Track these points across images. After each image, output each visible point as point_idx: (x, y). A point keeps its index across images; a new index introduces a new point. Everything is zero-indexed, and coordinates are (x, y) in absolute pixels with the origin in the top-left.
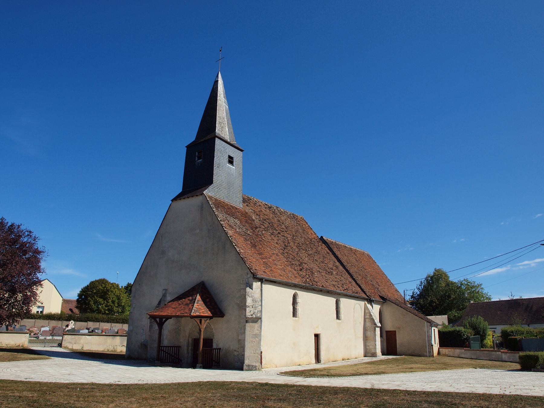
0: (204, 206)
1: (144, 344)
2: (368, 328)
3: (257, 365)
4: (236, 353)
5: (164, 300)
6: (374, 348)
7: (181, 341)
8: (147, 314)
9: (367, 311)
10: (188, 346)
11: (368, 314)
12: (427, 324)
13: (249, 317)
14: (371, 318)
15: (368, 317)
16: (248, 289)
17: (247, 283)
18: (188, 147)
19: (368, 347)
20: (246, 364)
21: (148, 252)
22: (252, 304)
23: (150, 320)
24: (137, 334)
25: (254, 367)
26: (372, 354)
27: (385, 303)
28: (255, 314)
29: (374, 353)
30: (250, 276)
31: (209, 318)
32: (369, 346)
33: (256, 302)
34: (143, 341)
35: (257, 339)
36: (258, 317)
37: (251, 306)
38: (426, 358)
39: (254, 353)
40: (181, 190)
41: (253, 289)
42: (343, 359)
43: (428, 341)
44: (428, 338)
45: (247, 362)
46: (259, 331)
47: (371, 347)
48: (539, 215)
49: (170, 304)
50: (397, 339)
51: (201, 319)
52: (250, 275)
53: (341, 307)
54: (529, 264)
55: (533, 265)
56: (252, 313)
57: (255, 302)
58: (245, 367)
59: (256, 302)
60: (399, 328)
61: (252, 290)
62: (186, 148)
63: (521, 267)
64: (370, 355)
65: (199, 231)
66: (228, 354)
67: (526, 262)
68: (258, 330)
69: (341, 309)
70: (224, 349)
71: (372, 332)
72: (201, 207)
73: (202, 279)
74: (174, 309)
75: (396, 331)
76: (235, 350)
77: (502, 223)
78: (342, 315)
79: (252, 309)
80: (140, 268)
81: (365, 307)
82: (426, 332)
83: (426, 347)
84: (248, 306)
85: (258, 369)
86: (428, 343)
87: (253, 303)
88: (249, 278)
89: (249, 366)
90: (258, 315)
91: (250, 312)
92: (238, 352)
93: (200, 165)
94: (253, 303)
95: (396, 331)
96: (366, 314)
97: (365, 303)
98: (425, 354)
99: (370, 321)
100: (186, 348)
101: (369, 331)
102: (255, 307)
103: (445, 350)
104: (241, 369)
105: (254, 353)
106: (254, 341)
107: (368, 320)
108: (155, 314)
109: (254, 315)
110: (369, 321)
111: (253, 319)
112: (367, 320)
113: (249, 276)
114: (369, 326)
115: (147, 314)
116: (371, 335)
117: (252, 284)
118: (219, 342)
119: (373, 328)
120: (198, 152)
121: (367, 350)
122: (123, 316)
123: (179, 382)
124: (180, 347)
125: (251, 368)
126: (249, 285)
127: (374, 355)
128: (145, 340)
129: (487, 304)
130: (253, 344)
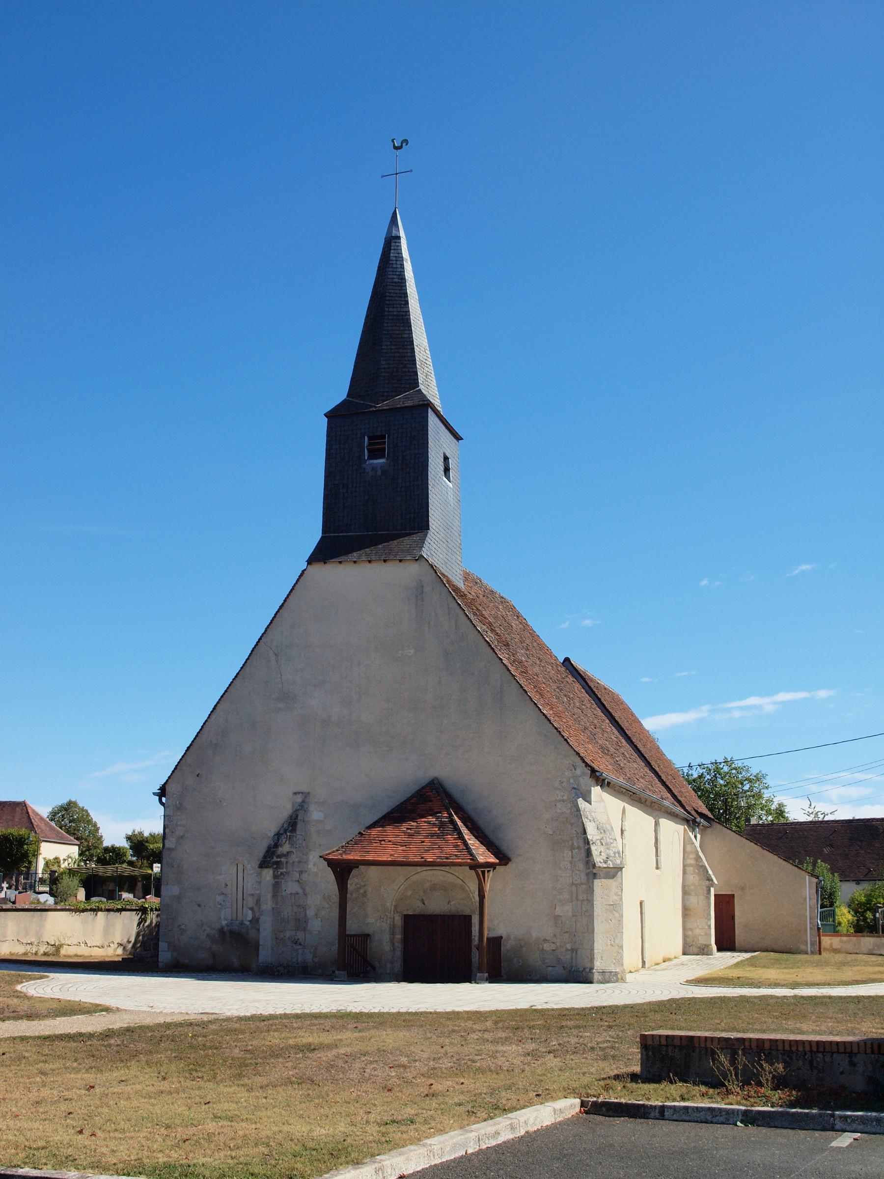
0: (427, 589)
1: (232, 933)
2: (692, 887)
3: (618, 970)
4: (547, 947)
5: (304, 821)
6: (706, 934)
7: (371, 920)
8: (321, 857)
9: (689, 848)
10: (393, 934)
11: (693, 856)
12: (809, 879)
13: (601, 865)
14: (700, 864)
15: (693, 862)
16: (581, 802)
17: (574, 788)
18: (331, 415)
19: (690, 933)
20: (597, 970)
21: (226, 691)
22: (598, 837)
23: (274, 872)
24: (199, 905)
25: (614, 975)
26: (700, 948)
27: (709, 830)
28: (611, 858)
29: (705, 945)
30: (583, 774)
31: (491, 868)
32: (691, 930)
33: (604, 831)
34: (224, 923)
35: (617, 915)
36: (618, 865)
37: (598, 841)
38: (805, 956)
39: (611, 945)
40: (320, 535)
41: (592, 803)
42: (663, 958)
43: (810, 919)
44: (810, 911)
45: (598, 965)
46: (618, 897)
47: (698, 931)
48: (804, 567)
49: (374, 832)
50: (736, 913)
51: (484, 871)
52: (581, 769)
53: (661, 837)
54: (758, 707)
55: (770, 708)
56: (604, 856)
57: (602, 831)
58: (596, 976)
59: (604, 831)
60: (743, 889)
61: (591, 804)
62: (326, 419)
63: (737, 714)
64: (696, 950)
65: (412, 651)
66: (524, 949)
67: (753, 701)
68: (616, 894)
69: (660, 844)
70: (512, 937)
71: (702, 897)
72: (419, 592)
73: (432, 773)
74: (402, 846)
75: (733, 895)
76: (545, 940)
77: (704, 583)
78: (662, 858)
79: (602, 849)
80: (198, 733)
81: (686, 839)
82: (806, 898)
83: (806, 931)
84: (592, 840)
85: (622, 979)
86: (810, 923)
87: (601, 836)
88: (580, 777)
89: (603, 972)
90: (617, 861)
91: (600, 855)
92: (554, 943)
93: (379, 473)
94: (601, 836)
95: (733, 895)
96: (686, 855)
97: (685, 828)
98: (802, 947)
99: (697, 871)
100: (387, 937)
101: (693, 893)
102: (606, 844)
103: (831, 939)
104: (588, 981)
105: (611, 945)
106: (610, 918)
107: (691, 868)
108: (345, 857)
109: (609, 862)
110: (694, 871)
111: (608, 870)
112: (690, 869)
113: (578, 772)
114: (693, 884)
115: (321, 857)
116: (698, 904)
117: (590, 792)
118: (496, 923)
119: (704, 887)
120: (368, 436)
121: (688, 940)
122: (269, 859)
123: (651, 1000)
124: (369, 935)
125: (609, 978)
126: (581, 793)
127: (705, 949)
128: (232, 920)
129: (795, 828)
130: (608, 926)
